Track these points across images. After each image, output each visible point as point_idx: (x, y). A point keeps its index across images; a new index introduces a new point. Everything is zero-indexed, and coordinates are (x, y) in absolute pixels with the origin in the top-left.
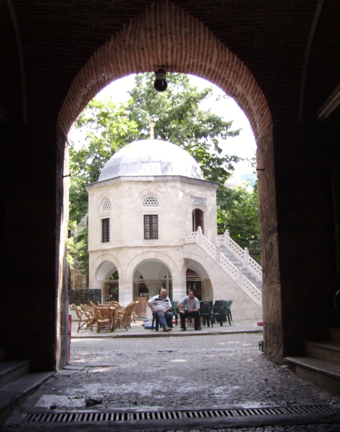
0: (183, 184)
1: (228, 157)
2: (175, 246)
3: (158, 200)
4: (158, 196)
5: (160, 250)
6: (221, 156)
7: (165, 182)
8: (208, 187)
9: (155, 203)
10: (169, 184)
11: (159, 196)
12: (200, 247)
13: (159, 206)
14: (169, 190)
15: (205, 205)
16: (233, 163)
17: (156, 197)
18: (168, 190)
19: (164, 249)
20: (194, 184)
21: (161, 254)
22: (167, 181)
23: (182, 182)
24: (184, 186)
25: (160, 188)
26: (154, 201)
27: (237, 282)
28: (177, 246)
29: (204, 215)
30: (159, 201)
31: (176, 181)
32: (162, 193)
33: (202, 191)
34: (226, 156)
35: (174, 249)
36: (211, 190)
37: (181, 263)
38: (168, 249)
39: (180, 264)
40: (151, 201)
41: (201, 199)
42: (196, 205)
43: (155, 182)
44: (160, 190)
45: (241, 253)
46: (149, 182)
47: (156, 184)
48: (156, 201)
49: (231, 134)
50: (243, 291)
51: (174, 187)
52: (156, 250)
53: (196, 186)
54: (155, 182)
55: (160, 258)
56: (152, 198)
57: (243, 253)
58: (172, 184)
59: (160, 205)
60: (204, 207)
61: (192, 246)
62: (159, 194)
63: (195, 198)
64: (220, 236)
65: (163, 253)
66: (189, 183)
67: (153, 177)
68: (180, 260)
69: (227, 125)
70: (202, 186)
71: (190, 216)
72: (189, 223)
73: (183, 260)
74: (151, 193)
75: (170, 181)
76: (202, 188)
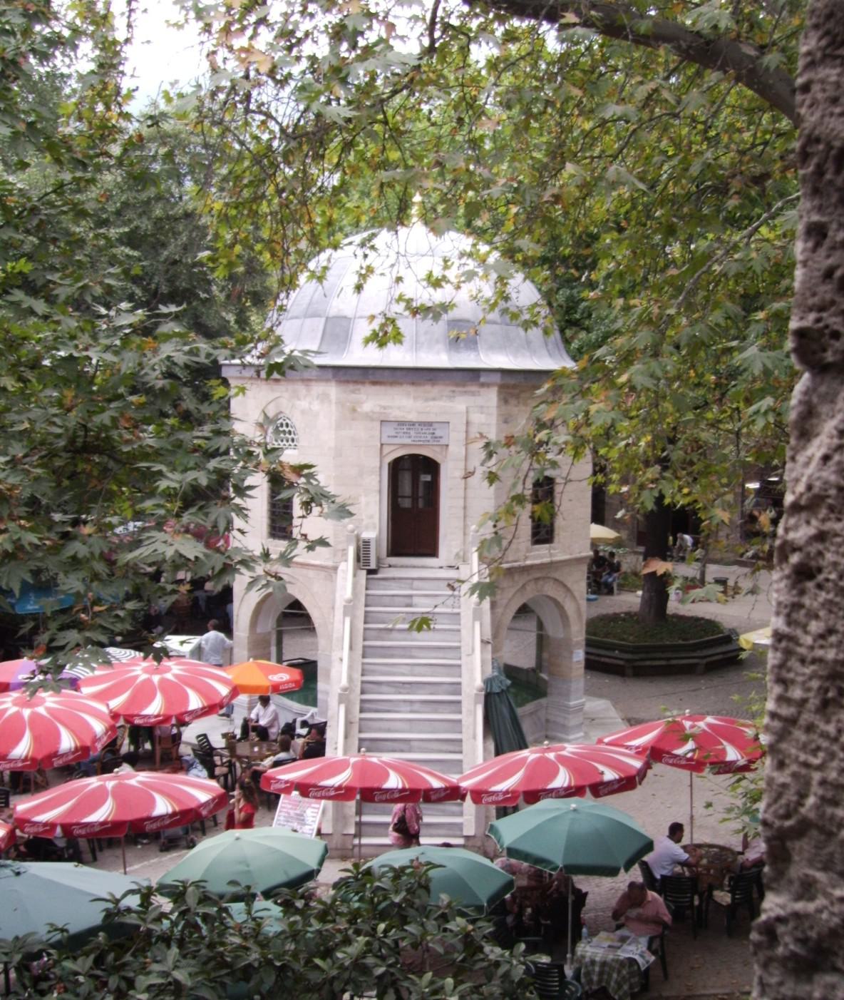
0: (351, 387)
10: (318, 388)
11: (297, 421)
14: (316, 406)
15: (443, 442)
24: (353, 392)
32: (303, 412)
33: (434, 399)
35: (323, 574)
38: (311, 573)
41: (430, 424)
42: (404, 446)
51: (324, 398)
53: (411, 389)
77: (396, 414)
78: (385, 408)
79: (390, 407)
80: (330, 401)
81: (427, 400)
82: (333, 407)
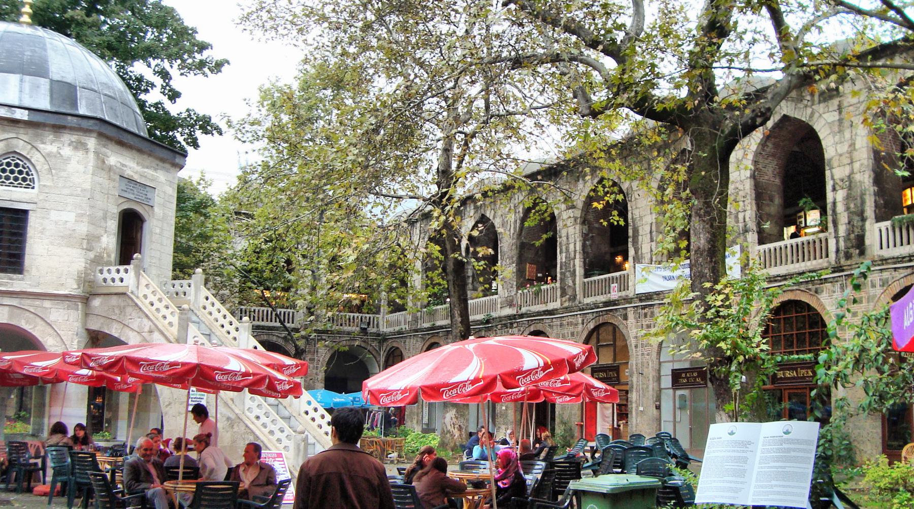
0: (104, 141)
1: (189, 115)
2: (66, 296)
3: (33, 172)
4: (33, 160)
5: (26, 303)
6: (175, 109)
7: (58, 129)
8: (163, 160)
9: (24, 180)
10: (67, 137)
12: (136, 305)
13: (33, 188)
14: (67, 151)
16: (198, 134)
17: (28, 164)
18: (62, 152)
19: (38, 302)
20: (129, 147)
21: (28, 314)
22: (64, 127)
23: (101, 135)
25: (43, 143)
26: (20, 172)
27: (230, 403)
28: (73, 297)
29: (147, 227)
30: (35, 176)
31: (87, 131)
32: (46, 157)
34: (188, 110)
36: (168, 171)
37: (78, 342)
38: (47, 304)
39: (75, 342)
40: (12, 172)
42: (129, 200)
43: (29, 124)
44: (41, 146)
45: (232, 329)
46: (15, 122)
47: (31, 131)
48: (27, 174)
49: (202, 64)
50: (247, 426)
51: (80, 146)
52: (14, 302)
54: (29, 124)
55: (24, 325)
56: (17, 165)
57: (237, 329)
58: (74, 138)
59: (36, 185)
60: (147, 208)
61: (114, 300)
62: (36, 158)
63: (130, 180)
64: (177, 282)
65: (33, 311)
66: (121, 143)
67: (27, 112)
68: (77, 335)
69: (203, 47)
70: (150, 155)
71: (113, 225)
72: (110, 241)
73: (84, 334)
74: (15, 152)
75: (72, 129)
76: (148, 161)
77: (128, 173)
78: (123, 165)
79: (126, 166)
80: (87, 150)
81: (144, 167)
82: (91, 155)
